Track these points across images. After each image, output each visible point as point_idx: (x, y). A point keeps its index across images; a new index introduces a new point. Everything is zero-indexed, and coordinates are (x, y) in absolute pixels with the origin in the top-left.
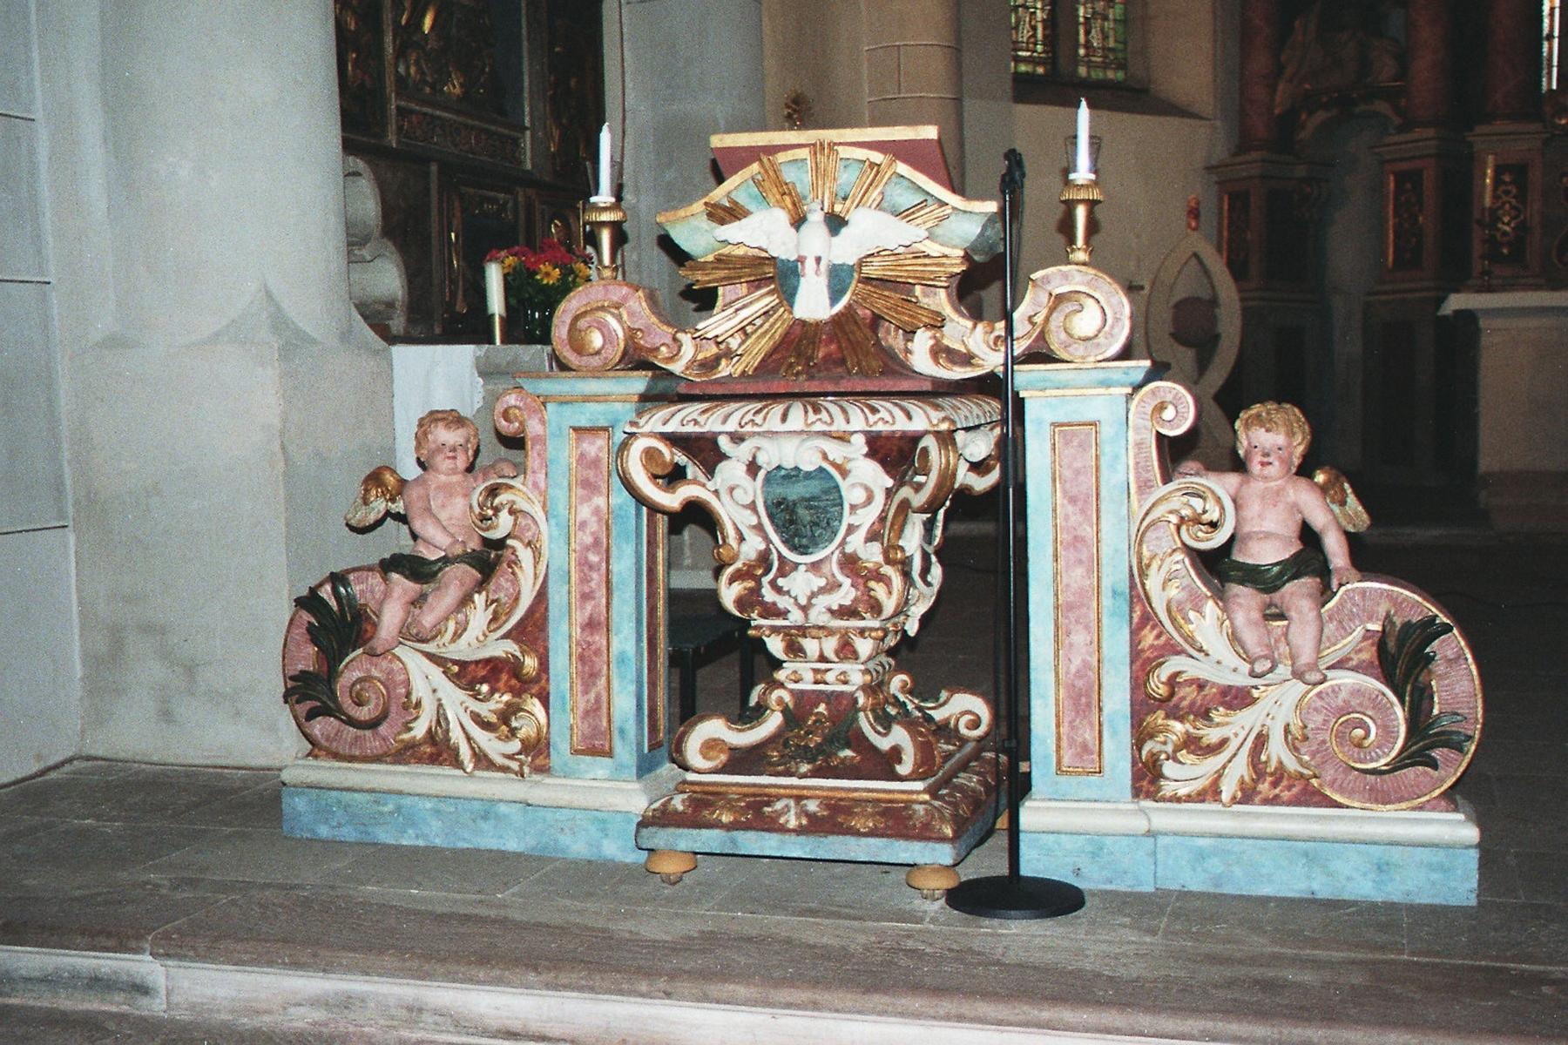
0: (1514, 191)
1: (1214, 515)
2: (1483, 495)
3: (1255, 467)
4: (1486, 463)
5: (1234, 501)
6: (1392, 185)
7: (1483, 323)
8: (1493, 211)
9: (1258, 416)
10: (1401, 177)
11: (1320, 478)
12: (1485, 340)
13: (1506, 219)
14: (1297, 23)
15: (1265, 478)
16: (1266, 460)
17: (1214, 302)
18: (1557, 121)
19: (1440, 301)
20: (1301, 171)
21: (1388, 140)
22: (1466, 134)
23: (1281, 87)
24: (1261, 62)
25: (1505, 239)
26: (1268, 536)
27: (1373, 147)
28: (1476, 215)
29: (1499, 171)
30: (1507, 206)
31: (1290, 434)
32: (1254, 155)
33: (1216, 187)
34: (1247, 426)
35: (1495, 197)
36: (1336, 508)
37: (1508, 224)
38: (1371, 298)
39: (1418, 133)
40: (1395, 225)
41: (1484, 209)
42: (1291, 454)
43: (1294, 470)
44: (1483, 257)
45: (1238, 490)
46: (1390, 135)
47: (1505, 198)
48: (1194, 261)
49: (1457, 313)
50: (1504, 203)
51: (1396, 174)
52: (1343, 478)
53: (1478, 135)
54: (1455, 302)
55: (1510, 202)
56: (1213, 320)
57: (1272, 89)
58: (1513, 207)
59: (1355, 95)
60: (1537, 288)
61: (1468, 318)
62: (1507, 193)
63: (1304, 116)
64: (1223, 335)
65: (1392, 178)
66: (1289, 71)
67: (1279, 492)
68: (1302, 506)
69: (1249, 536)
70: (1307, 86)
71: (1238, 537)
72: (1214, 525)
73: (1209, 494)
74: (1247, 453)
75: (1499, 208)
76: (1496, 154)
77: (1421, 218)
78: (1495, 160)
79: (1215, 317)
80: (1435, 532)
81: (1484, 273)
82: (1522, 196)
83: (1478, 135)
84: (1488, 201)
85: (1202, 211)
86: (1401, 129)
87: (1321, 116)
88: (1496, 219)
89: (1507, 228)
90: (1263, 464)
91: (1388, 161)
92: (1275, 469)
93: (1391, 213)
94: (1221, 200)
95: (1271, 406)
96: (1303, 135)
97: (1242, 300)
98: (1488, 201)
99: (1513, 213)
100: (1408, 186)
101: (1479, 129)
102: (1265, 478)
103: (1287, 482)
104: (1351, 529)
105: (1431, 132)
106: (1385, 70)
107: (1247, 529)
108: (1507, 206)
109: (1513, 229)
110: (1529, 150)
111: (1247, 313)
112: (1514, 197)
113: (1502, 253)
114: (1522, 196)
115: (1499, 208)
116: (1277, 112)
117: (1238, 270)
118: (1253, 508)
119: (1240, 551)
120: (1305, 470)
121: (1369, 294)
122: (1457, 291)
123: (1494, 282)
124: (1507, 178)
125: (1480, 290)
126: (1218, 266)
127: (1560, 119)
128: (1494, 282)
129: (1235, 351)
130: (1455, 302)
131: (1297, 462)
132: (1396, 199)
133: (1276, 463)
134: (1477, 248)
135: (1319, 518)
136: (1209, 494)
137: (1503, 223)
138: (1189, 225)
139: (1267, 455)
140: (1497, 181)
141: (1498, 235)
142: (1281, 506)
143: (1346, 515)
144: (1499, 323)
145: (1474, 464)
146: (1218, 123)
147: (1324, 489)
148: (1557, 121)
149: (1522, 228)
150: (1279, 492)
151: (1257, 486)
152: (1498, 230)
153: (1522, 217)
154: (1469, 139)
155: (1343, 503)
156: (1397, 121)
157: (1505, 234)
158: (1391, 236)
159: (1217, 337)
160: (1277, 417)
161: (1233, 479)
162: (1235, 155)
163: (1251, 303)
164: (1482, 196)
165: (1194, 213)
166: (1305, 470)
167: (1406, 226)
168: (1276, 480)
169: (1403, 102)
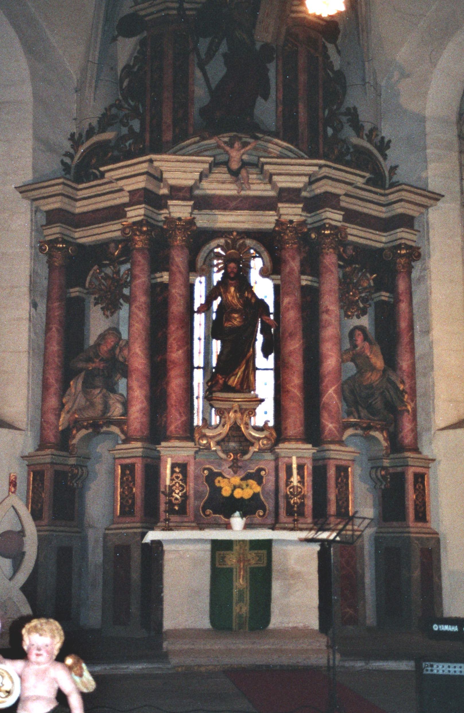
0: (181, 477)
1: (7, 687)
2: (165, 645)
3: (33, 657)
4: (168, 624)
5: (20, 676)
6: (120, 471)
7: (166, 547)
8: (170, 487)
9: (35, 627)
10: (124, 467)
11: (69, 661)
12: (167, 557)
13: (177, 491)
14: (72, 383)
15: (38, 663)
16: (39, 653)
17: (22, 533)
18: (201, 441)
19: (143, 535)
20: (72, 461)
21: (118, 447)
22: (157, 446)
23: (63, 415)
24: (53, 402)
25: (177, 502)
26: (38, 698)
27: (110, 451)
28: (162, 489)
29: (173, 466)
30: (177, 485)
31: (53, 637)
32: (49, 451)
33: (26, 468)
34: (29, 632)
35: (172, 480)
36: (77, 679)
37: (178, 494)
38: (107, 532)
39: (134, 444)
40: (120, 492)
41: (166, 486)
42: (53, 649)
43: (54, 657)
44: (166, 511)
45: (23, 670)
46: (119, 444)
47: (176, 480)
48: (12, 508)
49: (153, 542)
50: (176, 483)
51: (121, 465)
52: (81, 661)
53: (163, 447)
54: (152, 536)
55: (179, 483)
56: (21, 544)
57: (59, 416)
58: (180, 485)
59: (101, 422)
60: (193, 528)
61: (158, 544)
62: (177, 478)
63: (74, 432)
64: (27, 553)
65: (119, 467)
66: (67, 407)
67: (45, 671)
68: (59, 679)
69: (28, 699)
70: (77, 416)
71: (22, 698)
72: (9, 693)
73: (5, 674)
74: (29, 649)
75: (174, 485)
76: (171, 457)
77: (134, 489)
78: (172, 460)
79: (23, 541)
80: (139, 667)
81: (166, 520)
82: (185, 480)
83: (163, 447)
84: (168, 482)
85: (18, 482)
86: (125, 442)
87: (83, 432)
88: (172, 491)
89: (178, 497)
90: (38, 655)
91: (117, 458)
92: (44, 658)
93: (119, 486)
94: (29, 475)
95: (43, 621)
96: (74, 441)
97: (38, 531)
98: (168, 482)
99: (181, 488)
100: (128, 472)
101: (163, 444)
102: (38, 663)
103: (50, 665)
104: (85, 690)
105: (139, 444)
106: (117, 410)
107: (28, 693)
108: (177, 485)
109: (181, 497)
110: (188, 456)
111: (41, 539)
112: (181, 480)
113: (175, 509)
114: (185, 480)
115: (174, 485)
116: (60, 428)
117: (36, 515)
118: (31, 681)
119: (22, 708)
120: (60, 658)
121: (106, 529)
122: (152, 529)
123: (171, 524)
124: (177, 470)
125: (164, 529)
126: (25, 513)
127: (203, 441)
128: (171, 524)
129: (33, 562)
130: (152, 536)
131: (56, 652)
132: (122, 478)
133: (45, 654)
134: (163, 507)
135: (68, 688)
136: (5, 674)
137: (175, 493)
138: (10, 490)
139: (39, 649)
140: (173, 472)
141: (173, 499)
142: (47, 680)
143: (82, 682)
144: (173, 547)
145: (161, 625)
146: (29, 433)
147: (70, 668)
148: (201, 441)
149: (185, 497)
150: (45, 671)
151: (33, 668)
152: (173, 497)
153: (185, 491)
154: (158, 449)
155: (81, 675)
156: (123, 437)
157: (176, 499)
158: (119, 498)
159: (23, 554)
160: (46, 627)
161: (19, 664)
162: (37, 450)
163: (41, 533)
164: (165, 481)
165: (13, 483)
166: (60, 658)
167: (126, 493)
168: (44, 664)
169: (125, 428)
